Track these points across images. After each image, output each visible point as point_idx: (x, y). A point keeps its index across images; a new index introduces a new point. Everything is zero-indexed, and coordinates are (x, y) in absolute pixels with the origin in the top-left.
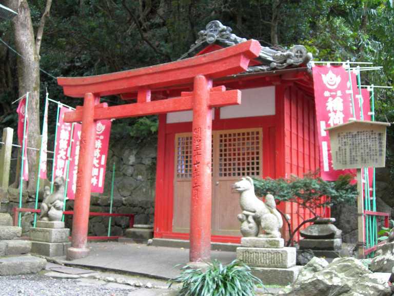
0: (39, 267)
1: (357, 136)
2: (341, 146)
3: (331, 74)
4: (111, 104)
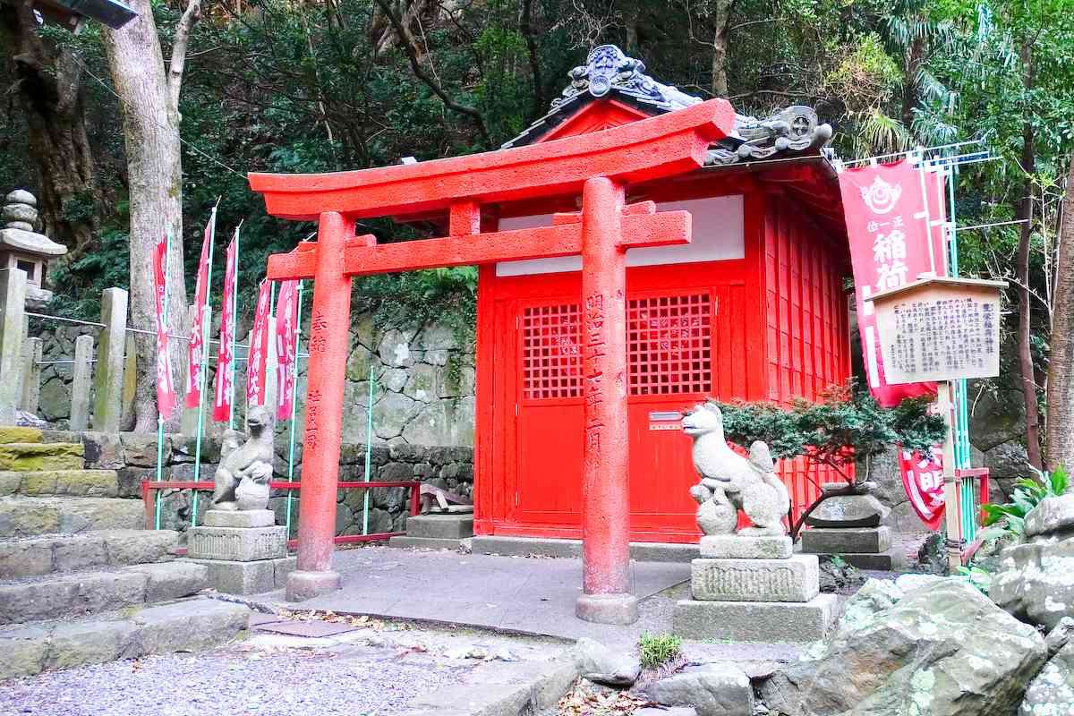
0: (232, 626)
1: (936, 311)
2: (901, 333)
3: (879, 183)
4: (382, 239)
